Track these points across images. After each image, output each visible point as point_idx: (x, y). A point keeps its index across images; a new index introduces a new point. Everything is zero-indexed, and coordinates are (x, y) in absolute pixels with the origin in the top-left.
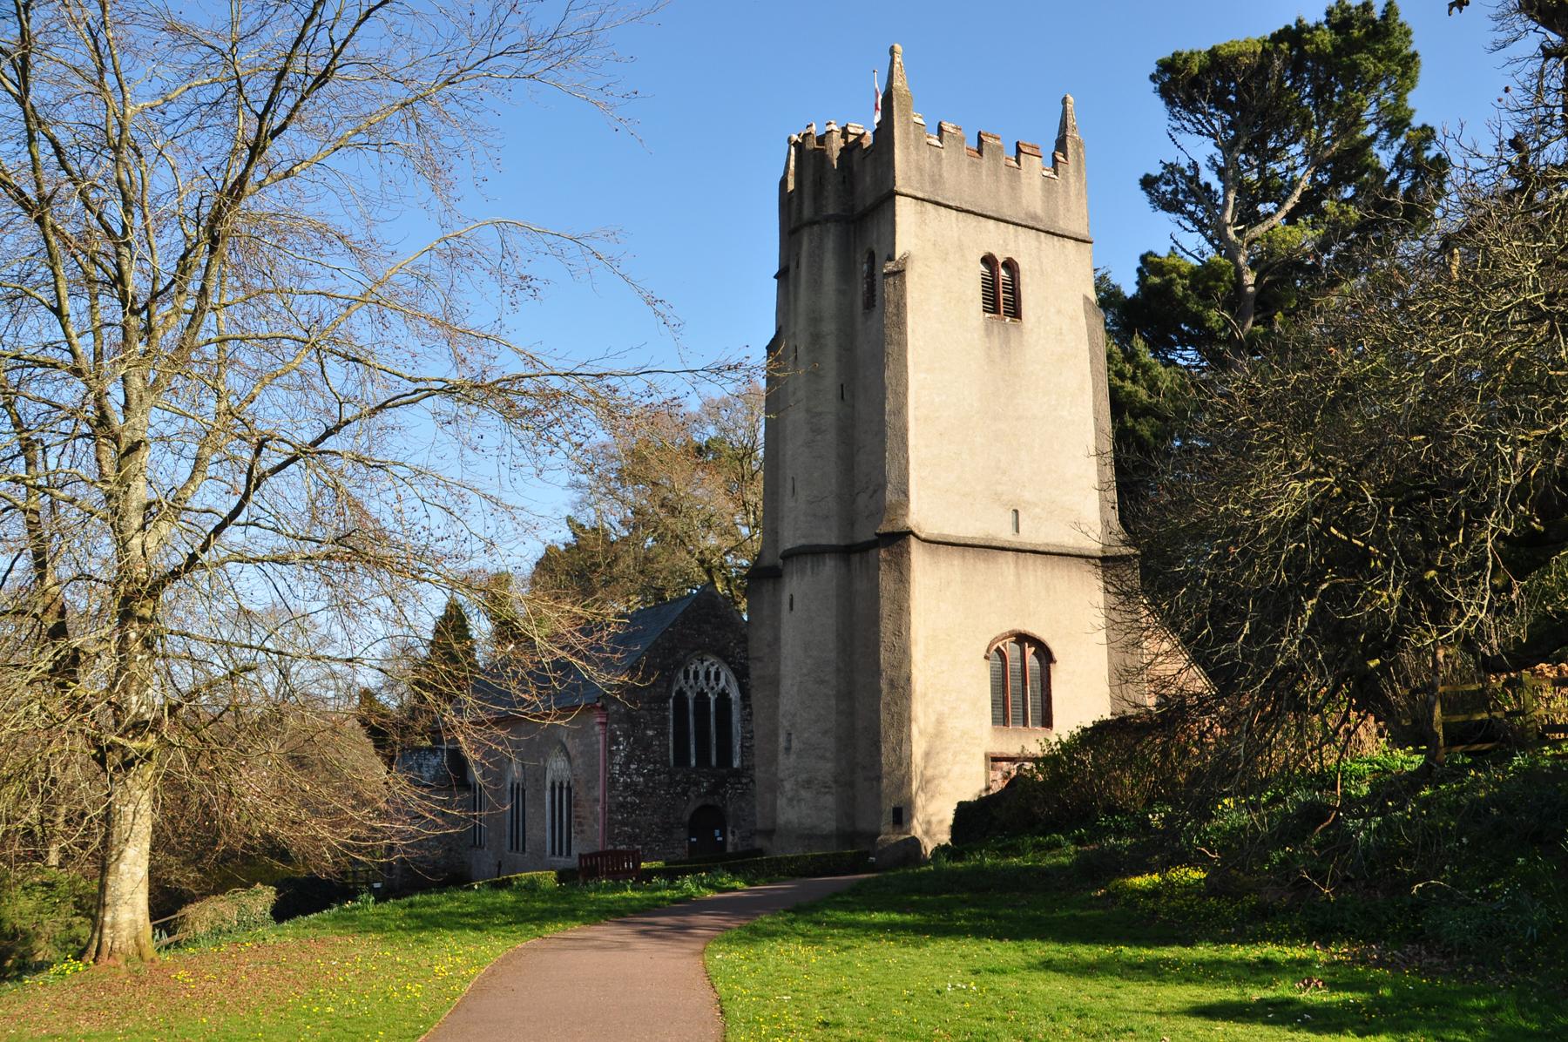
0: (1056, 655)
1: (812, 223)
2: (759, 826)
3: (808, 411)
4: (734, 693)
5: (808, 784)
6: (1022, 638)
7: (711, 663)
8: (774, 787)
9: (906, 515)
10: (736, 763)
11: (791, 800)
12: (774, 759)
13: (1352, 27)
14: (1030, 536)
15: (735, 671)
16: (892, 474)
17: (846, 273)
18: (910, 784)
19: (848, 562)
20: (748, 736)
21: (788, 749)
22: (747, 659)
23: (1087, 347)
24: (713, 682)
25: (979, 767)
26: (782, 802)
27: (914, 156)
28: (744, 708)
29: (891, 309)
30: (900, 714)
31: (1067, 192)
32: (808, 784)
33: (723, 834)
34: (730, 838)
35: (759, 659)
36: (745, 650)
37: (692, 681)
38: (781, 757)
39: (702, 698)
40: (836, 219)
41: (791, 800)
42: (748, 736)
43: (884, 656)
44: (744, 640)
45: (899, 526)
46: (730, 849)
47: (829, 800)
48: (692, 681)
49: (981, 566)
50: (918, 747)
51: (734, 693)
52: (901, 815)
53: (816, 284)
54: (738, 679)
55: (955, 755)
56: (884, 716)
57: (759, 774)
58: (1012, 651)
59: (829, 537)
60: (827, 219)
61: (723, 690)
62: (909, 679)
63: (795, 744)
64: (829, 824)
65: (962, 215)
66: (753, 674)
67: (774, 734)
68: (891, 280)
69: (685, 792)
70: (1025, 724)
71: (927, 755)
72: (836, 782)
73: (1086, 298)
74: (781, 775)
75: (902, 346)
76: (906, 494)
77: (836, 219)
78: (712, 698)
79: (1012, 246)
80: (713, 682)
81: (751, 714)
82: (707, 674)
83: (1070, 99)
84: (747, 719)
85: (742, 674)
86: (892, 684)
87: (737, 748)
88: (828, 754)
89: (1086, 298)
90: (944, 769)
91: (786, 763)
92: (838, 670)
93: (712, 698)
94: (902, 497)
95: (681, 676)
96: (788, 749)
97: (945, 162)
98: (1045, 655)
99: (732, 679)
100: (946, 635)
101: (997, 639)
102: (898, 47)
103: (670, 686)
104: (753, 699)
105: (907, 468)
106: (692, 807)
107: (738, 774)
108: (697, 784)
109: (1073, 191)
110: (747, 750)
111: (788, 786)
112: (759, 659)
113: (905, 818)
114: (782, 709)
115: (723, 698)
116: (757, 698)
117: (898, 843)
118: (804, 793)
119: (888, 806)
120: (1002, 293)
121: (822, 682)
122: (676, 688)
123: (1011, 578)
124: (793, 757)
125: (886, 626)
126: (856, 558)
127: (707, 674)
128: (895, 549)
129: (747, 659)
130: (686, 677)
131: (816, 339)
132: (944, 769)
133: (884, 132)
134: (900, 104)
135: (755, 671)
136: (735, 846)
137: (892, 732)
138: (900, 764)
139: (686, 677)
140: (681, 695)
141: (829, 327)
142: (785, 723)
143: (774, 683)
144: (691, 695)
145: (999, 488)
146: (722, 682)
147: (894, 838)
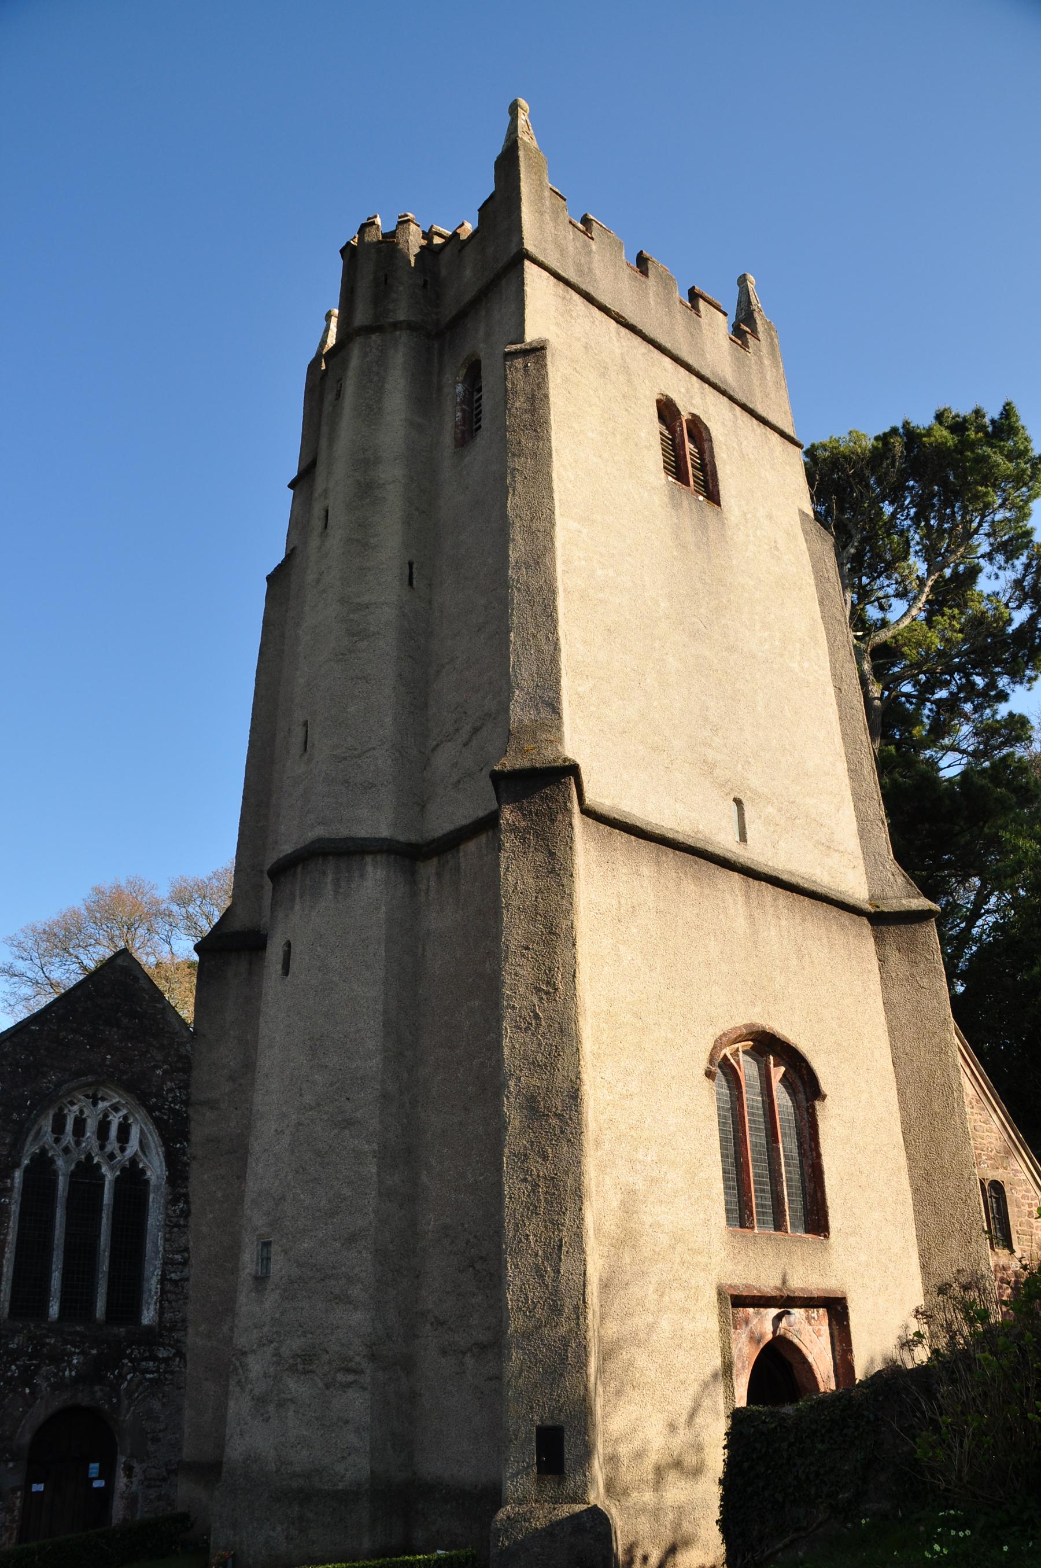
0: (825, 1086)
1: (367, 330)
2: (188, 1452)
3: (343, 600)
4: (155, 1169)
5: (305, 1362)
6: (766, 1044)
7: (114, 1105)
8: (225, 1367)
9: (560, 740)
10: (148, 1316)
11: (261, 1401)
12: (227, 1308)
13: (968, 430)
14: (759, 852)
15: (158, 1123)
16: (524, 673)
17: (425, 399)
18: (583, 1365)
19: (412, 877)
20: (177, 1260)
21: (260, 1280)
22: (187, 1103)
23: (812, 582)
24: (113, 1145)
25: (707, 1319)
26: (239, 1406)
27: (550, 227)
28: (174, 1201)
29: (519, 403)
30: (553, 1180)
31: (763, 378)
32: (305, 1362)
33: (108, 1474)
34: (121, 1481)
35: (212, 1105)
36: (186, 1086)
37: (68, 1138)
38: (245, 1302)
39: (86, 1174)
40: (411, 327)
41: (261, 1401)
42: (177, 1260)
43: (513, 1042)
44: (185, 1066)
45: (546, 757)
46: (118, 1510)
47: (356, 1403)
48: (68, 1138)
49: (690, 887)
50: (596, 1265)
51: (155, 1169)
52: (561, 1445)
53: (371, 412)
54: (167, 1140)
55: (661, 1291)
56: (512, 1186)
57: (194, 1339)
58: (747, 1069)
59: (377, 822)
60: (396, 326)
61: (134, 1161)
62: (574, 1096)
63: (279, 1266)
64: (352, 1462)
65: (624, 331)
66: (198, 1133)
67: (233, 1251)
68: (519, 363)
69: (27, 1376)
70: (779, 1225)
71: (605, 1286)
72: (372, 1357)
73: (802, 513)
74: (241, 1341)
75: (542, 459)
76: (554, 707)
77: (411, 327)
78: (109, 1175)
79: (697, 401)
80: (113, 1145)
81: (186, 1214)
82: (104, 1127)
83: (751, 278)
84: (177, 1224)
85: (174, 1133)
86: (533, 1107)
87: (152, 1283)
88: (355, 1291)
89: (802, 513)
90: (640, 1321)
91: (254, 1311)
92: (385, 1097)
93: (109, 1175)
94: (545, 713)
95: (47, 1124)
96: (260, 1280)
97: (596, 258)
98: (805, 1083)
99: (154, 1140)
100: (645, 1005)
101: (715, 1049)
102: (522, 102)
103: (17, 1146)
104: (194, 1182)
105: (555, 660)
106: (40, 1412)
107: (151, 1337)
108: (58, 1358)
109: (770, 374)
110: (173, 1289)
111: (256, 1366)
112: (212, 1105)
113: (569, 1456)
114: (252, 1187)
115: (132, 1178)
116: (201, 1181)
117: (554, 1529)
118: (294, 1386)
119: (523, 1422)
120: (689, 456)
121: (349, 1123)
122: (31, 1149)
123: (741, 923)
124: (271, 1299)
125: (518, 975)
126: (428, 869)
127: (104, 1127)
128: (536, 804)
129: (187, 1103)
130: (59, 1127)
131: (366, 491)
132: (640, 1321)
133: (501, 209)
134: (528, 158)
135: (203, 1127)
136: (132, 1501)
137: (533, 1227)
138: (556, 1310)
139: (59, 1127)
140: (42, 1163)
141: (392, 474)
142: (256, 1219)
143: (237, 1151)
144: (63, 1167)
145: (711, 754)
146: (133, 1146)
147: (542, 1516)
